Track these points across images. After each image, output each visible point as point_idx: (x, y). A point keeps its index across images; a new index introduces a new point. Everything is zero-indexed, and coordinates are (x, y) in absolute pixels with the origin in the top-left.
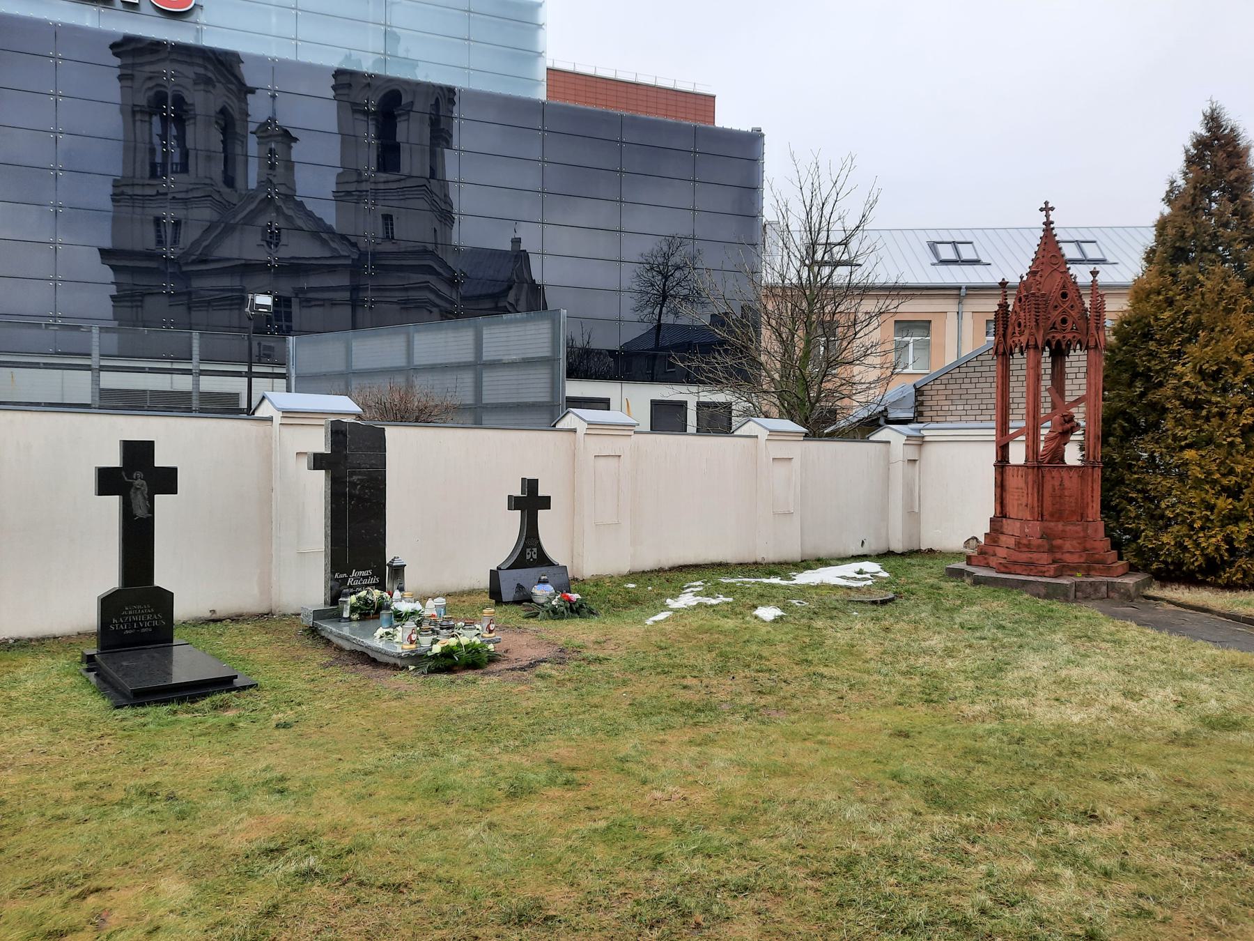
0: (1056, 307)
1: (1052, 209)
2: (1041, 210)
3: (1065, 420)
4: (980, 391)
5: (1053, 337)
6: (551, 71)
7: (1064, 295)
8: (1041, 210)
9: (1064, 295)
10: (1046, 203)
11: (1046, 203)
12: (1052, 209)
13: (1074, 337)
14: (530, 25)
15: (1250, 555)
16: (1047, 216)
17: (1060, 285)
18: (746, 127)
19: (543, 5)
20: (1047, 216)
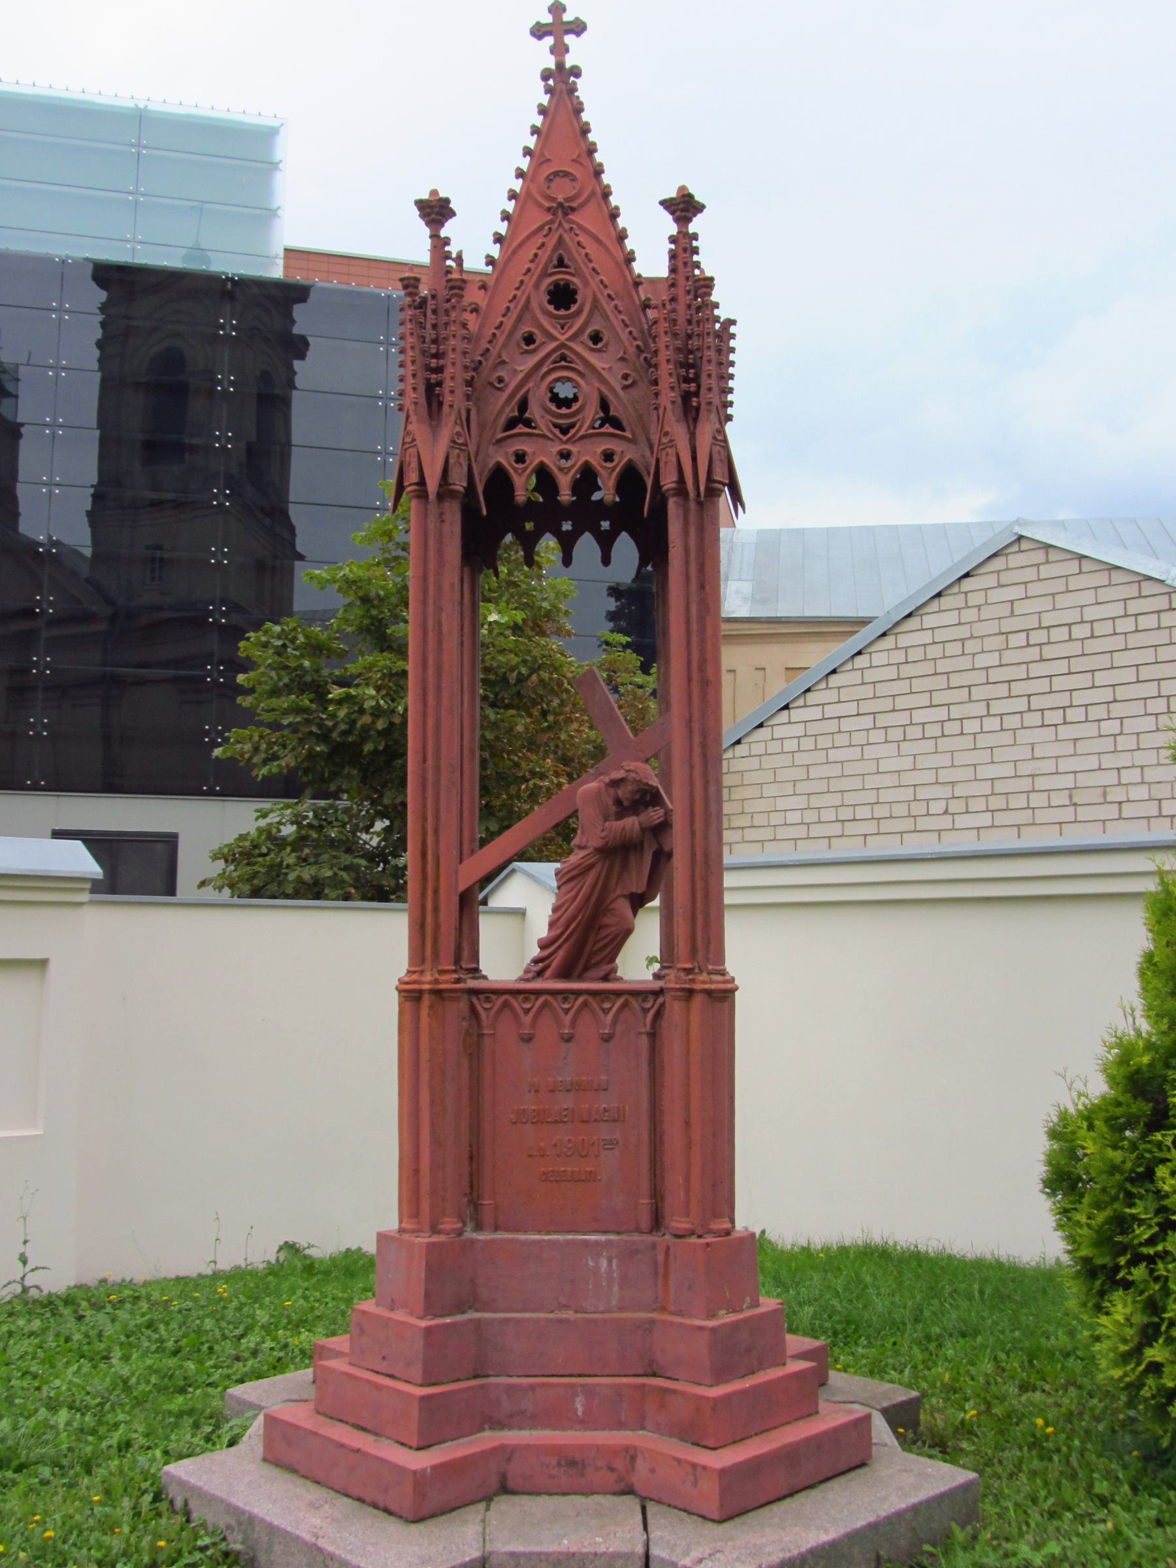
0: (529, 339)
1: (578, 28)
2: (539, 32)
3: (618, 802)
4: (1101, 678)
5: (520, 457)
6: (288, 251)
7: (562, 296)
8: (539, 32)
9: (562, 296)
10: (557, 9)
11: (557, 9)
12: (578, 28)
13: (608, 456)
14: (258, 165)
15: (1173, 1362)
16: (560, 50)
17: (544, 256)
18: (415, 208)
19: (282, 130)
20: (560, 50)
